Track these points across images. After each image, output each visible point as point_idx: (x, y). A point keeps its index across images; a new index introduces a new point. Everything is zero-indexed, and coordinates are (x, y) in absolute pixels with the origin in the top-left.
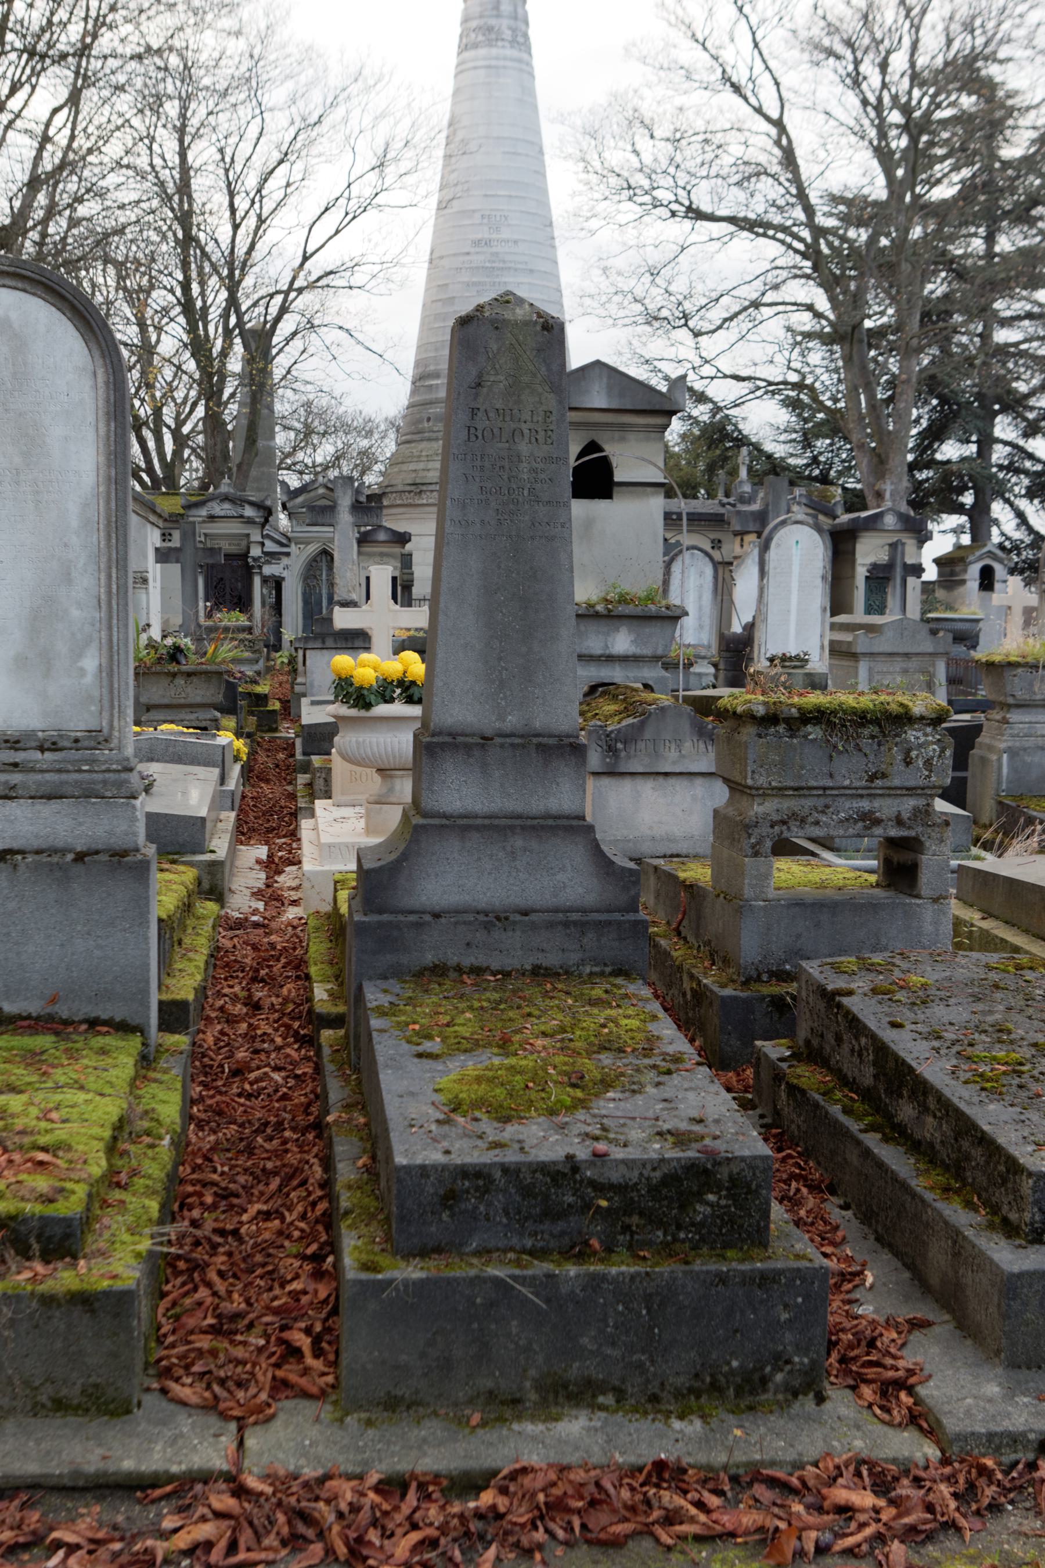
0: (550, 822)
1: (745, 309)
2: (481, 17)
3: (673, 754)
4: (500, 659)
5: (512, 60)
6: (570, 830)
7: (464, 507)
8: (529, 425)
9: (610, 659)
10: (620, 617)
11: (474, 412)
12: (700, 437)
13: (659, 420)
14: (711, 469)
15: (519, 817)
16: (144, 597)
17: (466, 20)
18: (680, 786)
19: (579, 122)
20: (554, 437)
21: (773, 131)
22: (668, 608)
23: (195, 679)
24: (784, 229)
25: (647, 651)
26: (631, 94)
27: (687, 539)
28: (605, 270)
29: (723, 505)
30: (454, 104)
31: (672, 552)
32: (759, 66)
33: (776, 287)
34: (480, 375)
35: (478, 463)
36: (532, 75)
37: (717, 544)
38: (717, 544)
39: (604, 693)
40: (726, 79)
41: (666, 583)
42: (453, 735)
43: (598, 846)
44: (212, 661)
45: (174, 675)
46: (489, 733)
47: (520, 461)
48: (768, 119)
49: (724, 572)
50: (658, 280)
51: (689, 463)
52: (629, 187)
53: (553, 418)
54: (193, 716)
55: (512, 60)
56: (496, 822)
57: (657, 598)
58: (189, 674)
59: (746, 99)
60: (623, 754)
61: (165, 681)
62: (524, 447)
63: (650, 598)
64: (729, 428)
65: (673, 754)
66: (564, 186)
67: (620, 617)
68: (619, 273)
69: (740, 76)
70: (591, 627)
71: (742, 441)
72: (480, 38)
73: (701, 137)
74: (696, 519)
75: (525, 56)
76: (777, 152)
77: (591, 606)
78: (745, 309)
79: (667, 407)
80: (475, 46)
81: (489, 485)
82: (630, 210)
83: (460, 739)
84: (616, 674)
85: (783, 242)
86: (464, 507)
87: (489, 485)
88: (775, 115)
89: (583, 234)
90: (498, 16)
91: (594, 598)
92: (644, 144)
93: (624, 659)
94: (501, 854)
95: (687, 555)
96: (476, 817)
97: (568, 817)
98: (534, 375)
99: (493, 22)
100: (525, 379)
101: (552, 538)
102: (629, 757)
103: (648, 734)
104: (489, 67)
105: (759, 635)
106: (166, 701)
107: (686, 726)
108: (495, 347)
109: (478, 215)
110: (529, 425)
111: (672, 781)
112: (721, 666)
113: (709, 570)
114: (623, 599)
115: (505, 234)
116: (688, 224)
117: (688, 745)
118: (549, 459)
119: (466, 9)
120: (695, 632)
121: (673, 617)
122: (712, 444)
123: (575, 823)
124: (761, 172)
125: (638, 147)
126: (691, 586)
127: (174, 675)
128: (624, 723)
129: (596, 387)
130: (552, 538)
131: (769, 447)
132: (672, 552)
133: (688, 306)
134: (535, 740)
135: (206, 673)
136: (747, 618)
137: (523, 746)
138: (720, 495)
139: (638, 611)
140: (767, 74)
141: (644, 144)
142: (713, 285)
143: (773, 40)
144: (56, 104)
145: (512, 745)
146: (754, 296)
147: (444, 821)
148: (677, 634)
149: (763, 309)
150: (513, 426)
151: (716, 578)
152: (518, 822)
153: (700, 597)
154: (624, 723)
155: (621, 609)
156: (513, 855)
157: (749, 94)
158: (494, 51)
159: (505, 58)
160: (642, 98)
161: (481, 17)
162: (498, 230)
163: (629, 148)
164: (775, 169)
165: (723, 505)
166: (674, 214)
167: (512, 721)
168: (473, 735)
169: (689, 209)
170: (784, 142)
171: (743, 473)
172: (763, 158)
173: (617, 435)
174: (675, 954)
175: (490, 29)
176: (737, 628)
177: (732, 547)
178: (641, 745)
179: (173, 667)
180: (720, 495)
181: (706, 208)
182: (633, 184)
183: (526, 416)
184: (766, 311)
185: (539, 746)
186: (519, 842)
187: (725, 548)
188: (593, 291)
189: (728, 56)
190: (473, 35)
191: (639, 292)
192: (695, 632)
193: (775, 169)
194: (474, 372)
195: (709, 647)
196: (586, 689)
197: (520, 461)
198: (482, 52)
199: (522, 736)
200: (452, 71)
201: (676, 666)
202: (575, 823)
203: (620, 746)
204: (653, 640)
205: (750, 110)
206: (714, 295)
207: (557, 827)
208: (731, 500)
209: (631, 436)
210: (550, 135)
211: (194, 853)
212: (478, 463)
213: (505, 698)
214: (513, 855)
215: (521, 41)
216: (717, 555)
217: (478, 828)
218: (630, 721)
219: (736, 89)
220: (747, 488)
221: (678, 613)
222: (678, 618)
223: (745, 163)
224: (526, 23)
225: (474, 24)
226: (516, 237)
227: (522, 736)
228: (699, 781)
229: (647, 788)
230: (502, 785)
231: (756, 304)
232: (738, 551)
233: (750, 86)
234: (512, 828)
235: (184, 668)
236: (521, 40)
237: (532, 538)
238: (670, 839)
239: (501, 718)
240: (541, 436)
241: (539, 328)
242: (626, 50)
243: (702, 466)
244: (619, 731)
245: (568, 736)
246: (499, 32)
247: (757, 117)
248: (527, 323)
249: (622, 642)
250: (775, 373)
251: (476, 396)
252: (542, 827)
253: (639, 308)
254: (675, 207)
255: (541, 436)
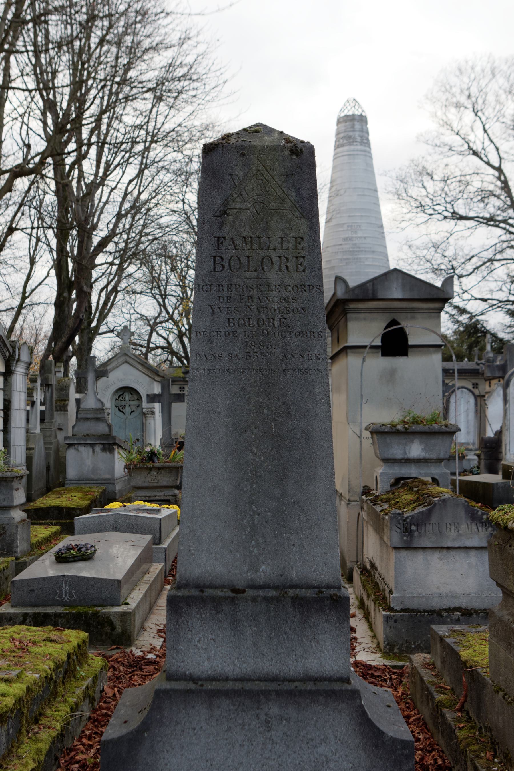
0: (310, 686)
1: (484, 263)
2: (345, 132)
3: (453, 533)
4: (251, 503)
5: (361, 151)
6: (331, 695)
7: (210, 340)
8: (278, 252)
9: (408, 461)
10: (414, 433)
11: (219, 241)
12: (464, 331)
13: (437, 305)
14: (470, 347)
15: (275, 679)
16: (152, 422)
17: (338, 134)
18: (459, 556)
19: (394, 175)
20: (306, 264)
21: (497, 174)
22: (446, 426)
23: (163, 471)
24: (505, 221)
25: (434, 456)
26: (421, 160)
27: (458, 383)
28: (410, 247)
29: (478, 364)
30: (333, 173)
31: (448, 391)
32: (487, 142)
33: (501, 252)
34: (226, 203)
35: (225, 294)
36: (371, 158)
37: (475, 386)
38: (475, 386)
39: (404, 485)
40: (470, 148)
41: (446, 409)
42: (201, 587)
43: (364, 713)
44: (173, 461)
45: (150, 469)
46: (240, 584)
47: (270, 290)
48: (493, 167)
49: (481, 401)
50: (439, 251)
51: (458, 346)
52: (422, 206)
53: (304, 244)
54: (162, 494)
55: (361, 151)
56: (248, 686)
57: (439, 420)
58: (159, 469)
59: (481, 159)
60: (416, 534)
61: (145, 473)
62: (273, 276)
63: (434, 420)
64: (479, 326)
65: (453, 533)
66: (389, 209)
67: (414, 433)
68: (418, 248)
69: (477, 147)
70: (394, 440)
71: (485, 332)
72: (345, 142)
73: (458, 179)
74: (462, 373)
75: (367, 149)
76: (499, 183)
77: (393, 426)
78: (484, 263)
79: (442, 296)
80: (343, 145)
81: (236, 316)
82: (422, 217)
83: (209, 592)
84: (412, 471)
85: (504, 229)
86: (210, 340)
87: (236, 316)
88: (497, 165)
89: (399, 230)
90: (354, 131)
91: (396, 421)
92: (429, 184)
93: (417, 461)
94: (254, 723)
95: (458, 392)
96: (227, 679)
97: (330, 680)
98: (283, 201)
99: (351, 134)
100: (274, 205)
101: (306, 371)
102: (420, 536)
103: (434, 518)
104: (350, 155)
105: (505, 439)
106: (146, 485)
107: (462, 513)
108: (241, 174)
109: (345, 226)
110: (278, 252)
111: (453, 553)
112: (482, 457)
113: (472, 400)
114: (416, 421)
115: (360, 234)
116: (453, 222)
117: (464, 526)
118: (301, 287)
119: (338, 129)
120: (466, 436)
121: (451, 432)
122: (470, 335)
123: (337, 687)
124: (492, 194)
125: (425, 184)
126: (462, 412)
127: (150, 469)
128: (417, 511)
129: (395, 285)
130: (306, 371)
131: (501, 335)
132: (448, 391)
133: (454, 263)
134: (291, 593)
135: (169, 467)
136: (497, 427)
137: (277, 600)
138: (476, 360)
139: (426, 428)
140: (492, 145)
141: (429, 184)
142: (467, 251)
143: (496, 129)
144: (131, 178)
145: (266, 599)
146: (490, 256)
147: (191, 686)
148: (454, 438)
149: (494, 262)
150: (262, 254)
151: (476, 404)
152: (273, 686)
153: (467, 416)
154: (417, 511)
155: (414, 428)
156: (268, 725)
157: (483, 156)
158: (352, 147)
159: (357, 151)
160: (427, 161)
161: (345, 132)
162: (356, 232)
163: (420, 185)
164: (498, 192)
165: (478, 364)
166: (445, 218)
167: (266, 571)
168: (222, 587)
169: (454, 213)
170: (503, 178)
171: (488, 347)
172: (491, 188)
173: (409, 315)
174: (458, 733)
175: (350, 137)
176: (490, 434)
177: (484, 387)
178: (429, 527)
179: (150, 465)
180: (476, 360)
181: (462, 212)
182: (423, 204)
183: (275, 243)
184: (497, 264)
185: (295, 599)
186: (274, 710)
187: (481, 387)
188: (404, 257)
189: (471, 138)
190: (341, 141)
191: (429, 257)
192: (466, 436)
193: (498, 192)
194: (219, 200)
195: (474, 444)
196: (393, 481)
197: (270, 290)
198: (346, 148)
199: (276, 588)
200: (331, 158)
201: (454, 458)
202: (337, 687)
203: (414, 528)
204: (439, 448)
205: (483, 163)
206: (468, 258)
207: (317, 692)
208: (483, 361)
209: (418, 315)
210: (381, 182)
211: (113, 605)
212: (225, 294)
213: (258, 545)
214: (268, 725)
215: (365, 142)
216: (476, 392)
217: (227, 694)
218: (420, 509)
219: (475, 153)
220: (491, 355)
221: (453, 429)
222: (454, 433)
223: (482, 191)
224: (367, 133)
225: (341, 135)
226: (365, 235)
227: (276, 588)
228: (473, 553)
229: (435, 558)
230: (255, 644)
231: (491, 260)
232: (487, 388)
233: (483, 152)
234: (266, 693)
235: (156, 465)
236: (365, 141)
237: (284, 371)
238: (454, 596)
239: (254, 567)
240: (292, 264)
241: (287, 153)
242: (418, 138)
243: (465, 347)
244: (413, 517)
245: (329, 587)
246: (354, 138)
247: (488, 167)
248: (274, 149)
249: (416, 450)
250: (502, 296)
251: (222, 225)
252: (301, 693)
253: (429, 265)
254: (446, 214)
255: (292, 264)
